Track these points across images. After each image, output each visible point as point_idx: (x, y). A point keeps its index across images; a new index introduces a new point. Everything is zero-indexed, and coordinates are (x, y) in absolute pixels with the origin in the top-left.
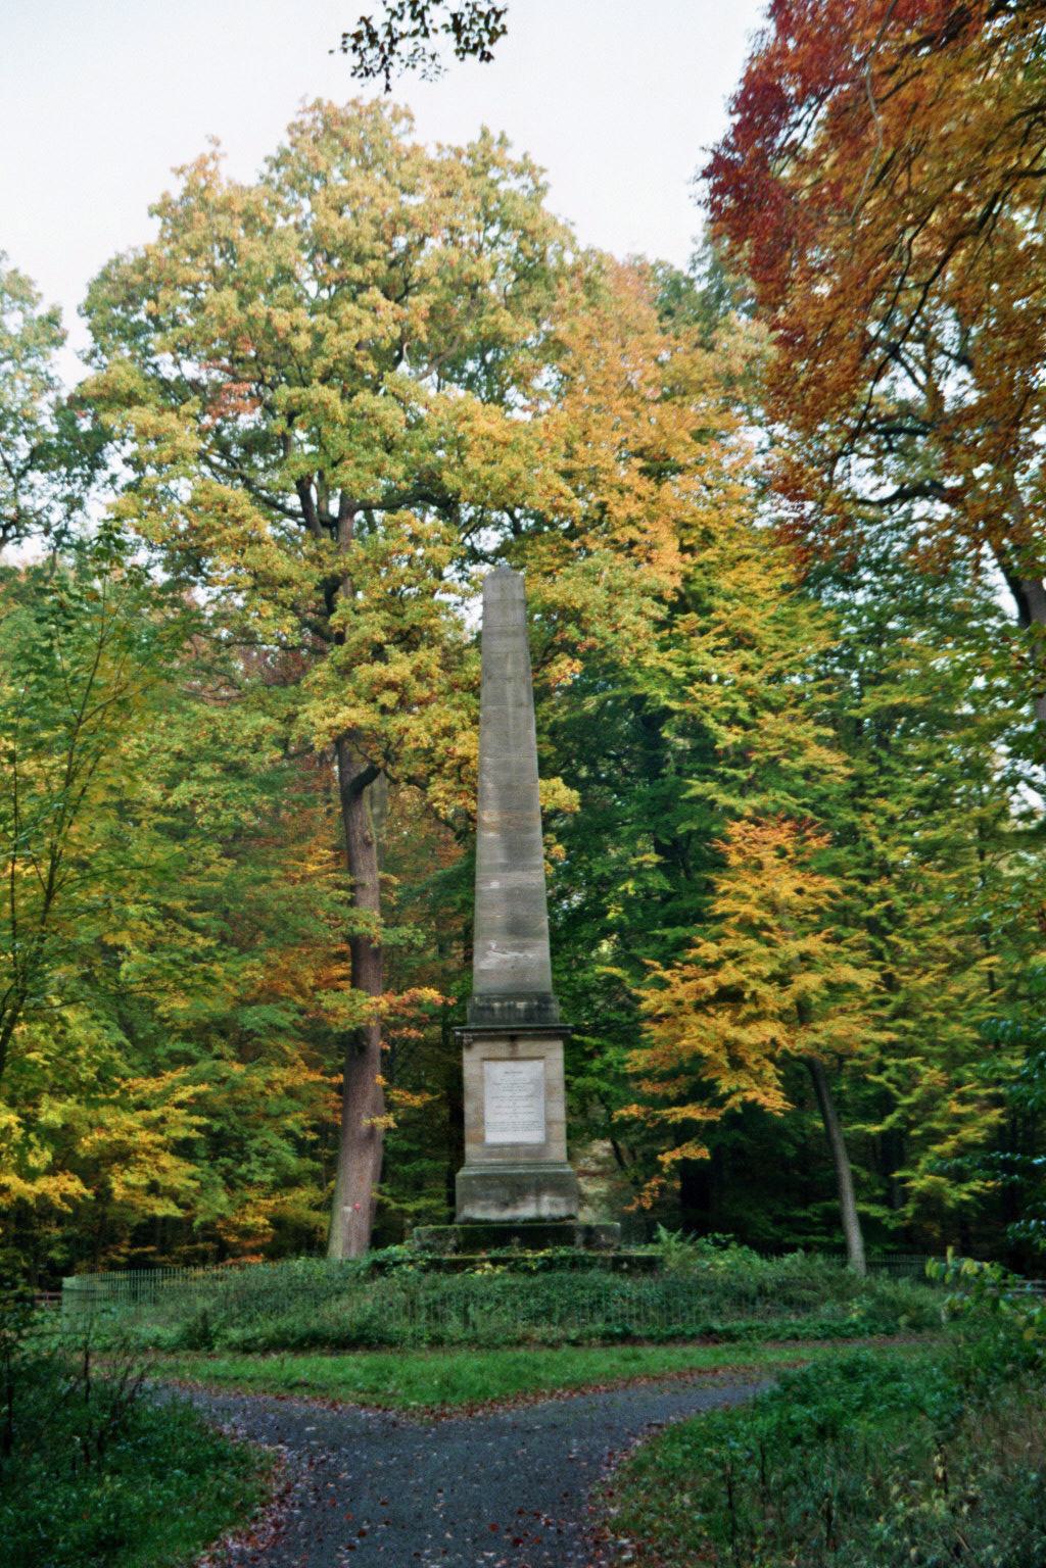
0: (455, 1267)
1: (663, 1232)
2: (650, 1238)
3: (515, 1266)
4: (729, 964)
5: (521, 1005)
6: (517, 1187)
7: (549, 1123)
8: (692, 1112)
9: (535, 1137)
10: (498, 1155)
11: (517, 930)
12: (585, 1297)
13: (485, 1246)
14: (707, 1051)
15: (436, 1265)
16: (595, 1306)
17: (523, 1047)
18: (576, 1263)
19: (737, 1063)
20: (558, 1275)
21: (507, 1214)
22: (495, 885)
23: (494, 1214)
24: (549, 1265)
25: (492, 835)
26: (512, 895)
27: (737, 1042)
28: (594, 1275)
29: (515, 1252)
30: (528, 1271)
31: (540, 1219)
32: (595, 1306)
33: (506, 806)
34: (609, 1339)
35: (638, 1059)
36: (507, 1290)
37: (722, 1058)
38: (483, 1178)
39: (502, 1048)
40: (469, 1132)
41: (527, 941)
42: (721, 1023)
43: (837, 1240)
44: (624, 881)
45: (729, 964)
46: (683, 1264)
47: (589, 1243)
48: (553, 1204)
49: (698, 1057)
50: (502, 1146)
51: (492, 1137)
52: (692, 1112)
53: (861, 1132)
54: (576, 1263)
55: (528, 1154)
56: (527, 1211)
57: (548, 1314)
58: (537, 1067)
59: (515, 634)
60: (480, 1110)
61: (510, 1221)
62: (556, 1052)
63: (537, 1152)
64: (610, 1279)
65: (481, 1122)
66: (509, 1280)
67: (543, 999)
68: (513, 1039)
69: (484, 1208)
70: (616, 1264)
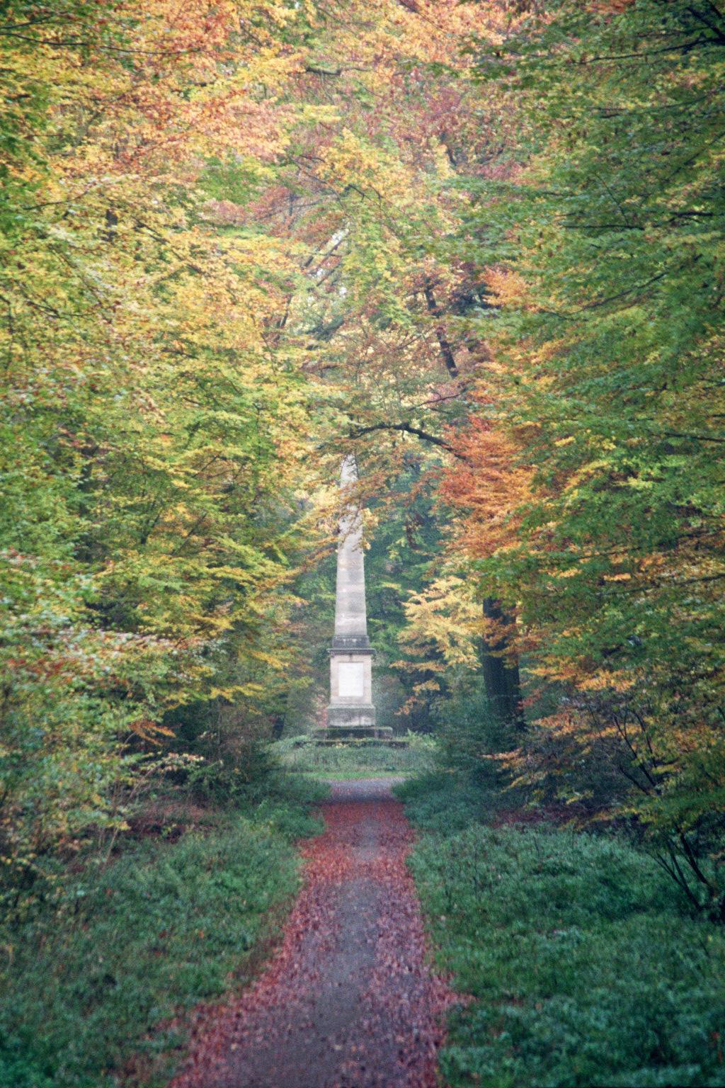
0: (329, 744)
1: (410, 732)
2: (404, 734)
3: (352, 745)
4: (451, 593)
6: (351, 714)
8: (431, 665)
9: (359, 694)
11: (353, 609)
12: (379, 756)
13: (339, 736)
14: (438, 638)
15: (320, 744)
16: (383, 760)
17: (355, 658)
18: (375, 744)
19: (454, 643)
20: (368, 748)
21: (348, 724)
23: (342, 724)
24: (365, 744)
26: (352, 595)
27: (454, 633)
28: (382, 748)
29: (351, 739)
30: (357, 747)
32: (383, 760)
34: (387, 770)
35: (404, 634)
36: (350, 754)
37: (447, 641)
38: (339, 710)
39: (346, 658)
40: (332, 692)
42: (446, 624)
44: (400, 537)
45: (451, 593)
46: (417, 744)
47: (380, 736)
49: (434, 641)
52: (431, 665)
54: (375, 744)
56: (355, 723)
57: (365, 762)
58: (361, 665)
60: (337, 682)
63: (360, 700)
64: (388, 750)
66: (350, 750)
67: (364, 639)
68: (351, 654)
70: (390, 745)
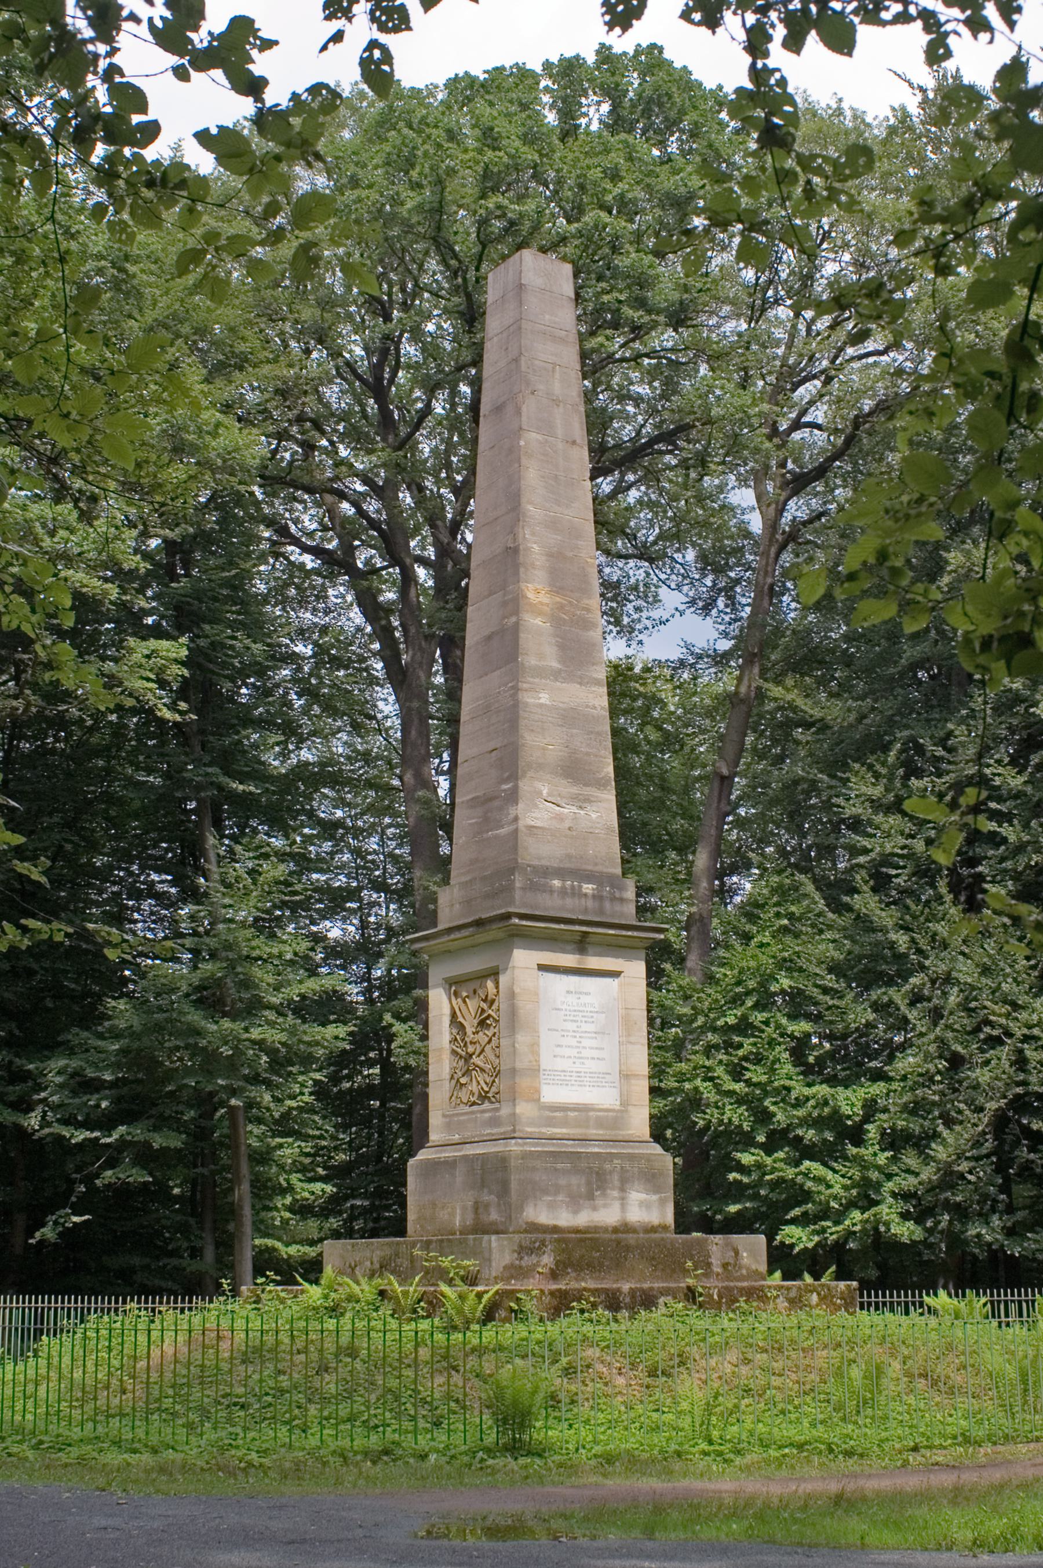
5: (588, 888)
7: (626, 1076)
10: (565, 1123)
11: (573, 770)
21: (583, 1219)
22: (544, 698)
25: (538, 621)
31: (625, 1228)
33: (557, 586)
41: (588, 791)
43: (661, 1103)
48: (645, 1205)
50: (564, 1108)
51: (552, 1094)
53: (274, 1249)
55: (600, 1123)
59: (563, 340)
61: (586, 1230)
62: (636, 969)
65: (535, 1071)
69: (552, 1206)
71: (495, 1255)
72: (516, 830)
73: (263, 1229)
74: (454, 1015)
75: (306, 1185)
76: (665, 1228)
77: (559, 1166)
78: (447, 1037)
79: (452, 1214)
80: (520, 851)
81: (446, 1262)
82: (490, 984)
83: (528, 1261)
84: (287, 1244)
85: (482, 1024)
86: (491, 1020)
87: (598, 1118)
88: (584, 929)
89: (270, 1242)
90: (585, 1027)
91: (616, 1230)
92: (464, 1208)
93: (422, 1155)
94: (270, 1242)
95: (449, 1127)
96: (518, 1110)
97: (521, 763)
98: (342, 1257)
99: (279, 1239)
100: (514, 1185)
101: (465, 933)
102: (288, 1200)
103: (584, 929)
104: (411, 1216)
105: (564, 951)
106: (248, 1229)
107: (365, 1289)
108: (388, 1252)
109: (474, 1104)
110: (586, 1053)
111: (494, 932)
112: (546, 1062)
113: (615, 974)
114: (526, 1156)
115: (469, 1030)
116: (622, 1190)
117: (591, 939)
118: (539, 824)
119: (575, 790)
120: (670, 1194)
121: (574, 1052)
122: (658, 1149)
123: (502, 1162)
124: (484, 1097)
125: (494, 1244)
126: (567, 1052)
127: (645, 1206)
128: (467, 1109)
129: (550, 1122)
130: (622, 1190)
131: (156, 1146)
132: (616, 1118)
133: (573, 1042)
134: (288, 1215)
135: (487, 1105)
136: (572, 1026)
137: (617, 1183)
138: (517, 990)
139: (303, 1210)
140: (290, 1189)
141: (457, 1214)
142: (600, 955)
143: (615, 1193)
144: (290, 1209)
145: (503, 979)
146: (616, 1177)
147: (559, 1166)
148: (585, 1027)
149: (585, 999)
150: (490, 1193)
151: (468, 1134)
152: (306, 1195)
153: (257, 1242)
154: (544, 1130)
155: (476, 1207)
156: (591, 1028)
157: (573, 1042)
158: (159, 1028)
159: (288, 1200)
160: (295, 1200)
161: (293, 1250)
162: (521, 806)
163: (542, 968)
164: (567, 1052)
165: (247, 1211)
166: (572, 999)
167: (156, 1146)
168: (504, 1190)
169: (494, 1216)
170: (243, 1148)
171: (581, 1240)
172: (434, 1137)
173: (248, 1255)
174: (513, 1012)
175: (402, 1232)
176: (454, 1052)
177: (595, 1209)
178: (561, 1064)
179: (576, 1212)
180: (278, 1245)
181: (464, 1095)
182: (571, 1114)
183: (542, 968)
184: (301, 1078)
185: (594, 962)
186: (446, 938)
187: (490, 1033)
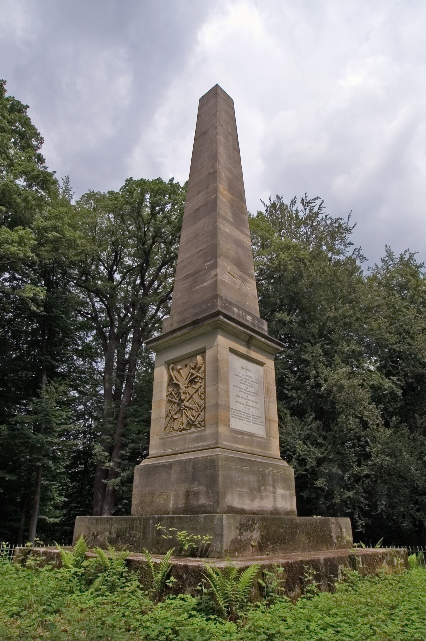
7: (268, 420)
31: (275, 512)
51: (236, 424)
53: (45, 519)
71: (226, 531)
72: (216, 281)
73: (42, 512)
74: (171, 379)
75: (59, 498)
76: (292, 512)
77: (244, 468)
78: (165, 393)
79: (167, 500)
80: (218, 290)
81: (182, 535)
82: (199, 358)
83: (246, 536)
84: (50, 518)
85: (192, 381)
86: (201, 376)
87: (258, 441)
88: (252, 333)
89: (44, 517)
90: (250, 389)
91: (272, 513)
92: (177, 496)
93: (145, 463)
94: (44, 517)
95: (164, 445)
96: (220, 430)
97: (219, 252)
98: (88, 528)
99: (47, 516)
100: (221, 479)
101: (184, 331)
102: (52, 503)
103: (252, 333)
104: (135, 502)
105: (241, 344)
106: (37, 512)
107: (112, 556)
108: (124, 525)
109: (183, 429)
110: (250, 403)
111: (206, 327)
112: (232, 405)
113: (261, 364)
114: (228, 459)
115: (182, 386)
116: (274, 487)
117: (253, 342)
118: (226, 281)
119: (241, 274)
120: (294, 491)
121: (244, 401)
122: (284, 463)
123: (212, 463)
124: (191, 424)
125: (225, 522)
126: (242, 401)
127: (283, 499)
128: (178, 433)
129: (236, 441)
130: (274, 487)
131: (7, 479)
132: (264, 444)
133: (244, 396)
134: (51, 508)
135: (193, 429)
136: (244, 387)
137: (271, 482)
138: (219, 358)
139: (56, 507)
140: (54, 499)
141: (171, 499)
142: (256, 352)
143: (270, 489)
144: (52, 506)
145: (209, 353)
146: (270, 478)
147: (244, 468)
148: (250, 389)
149: (249, 374)
150: (200, 484)
151: (178, 449)
152: (58, 501)
153: (40, 516)
154: (233, 445)
155: (187, 495)
156: (252, 390)
157: (244, 396)
158: (15, 437)
159: (52, 503)
160: (54, 503)
161: (51, 520)
162: (218, 270)
163: (232, 351)
164: (242, 401)
165: (38, 506)
166: (243, 371)
167: (7, 479)
168: (212, 482)
169: (203, 501)
170: (39, 483)
171: (275, 519)
172: (152, 452)
173: (36, 521)
174: (217, 370)
175: (128, 512)
176: (169, 401)
177: (262, 498)
178: (240, 407)
179: (253, 500)
180: (47, 518)
181: (176, 425)
182: (246, 437)
183: (232, 351)
184: (62, 463)
185: (254, 355)
186: (171, 337)
187: (197, 387)
